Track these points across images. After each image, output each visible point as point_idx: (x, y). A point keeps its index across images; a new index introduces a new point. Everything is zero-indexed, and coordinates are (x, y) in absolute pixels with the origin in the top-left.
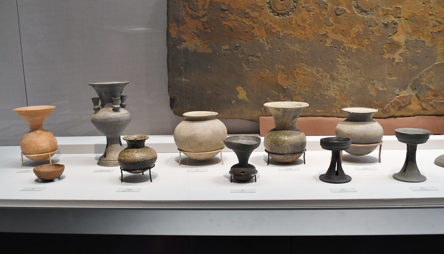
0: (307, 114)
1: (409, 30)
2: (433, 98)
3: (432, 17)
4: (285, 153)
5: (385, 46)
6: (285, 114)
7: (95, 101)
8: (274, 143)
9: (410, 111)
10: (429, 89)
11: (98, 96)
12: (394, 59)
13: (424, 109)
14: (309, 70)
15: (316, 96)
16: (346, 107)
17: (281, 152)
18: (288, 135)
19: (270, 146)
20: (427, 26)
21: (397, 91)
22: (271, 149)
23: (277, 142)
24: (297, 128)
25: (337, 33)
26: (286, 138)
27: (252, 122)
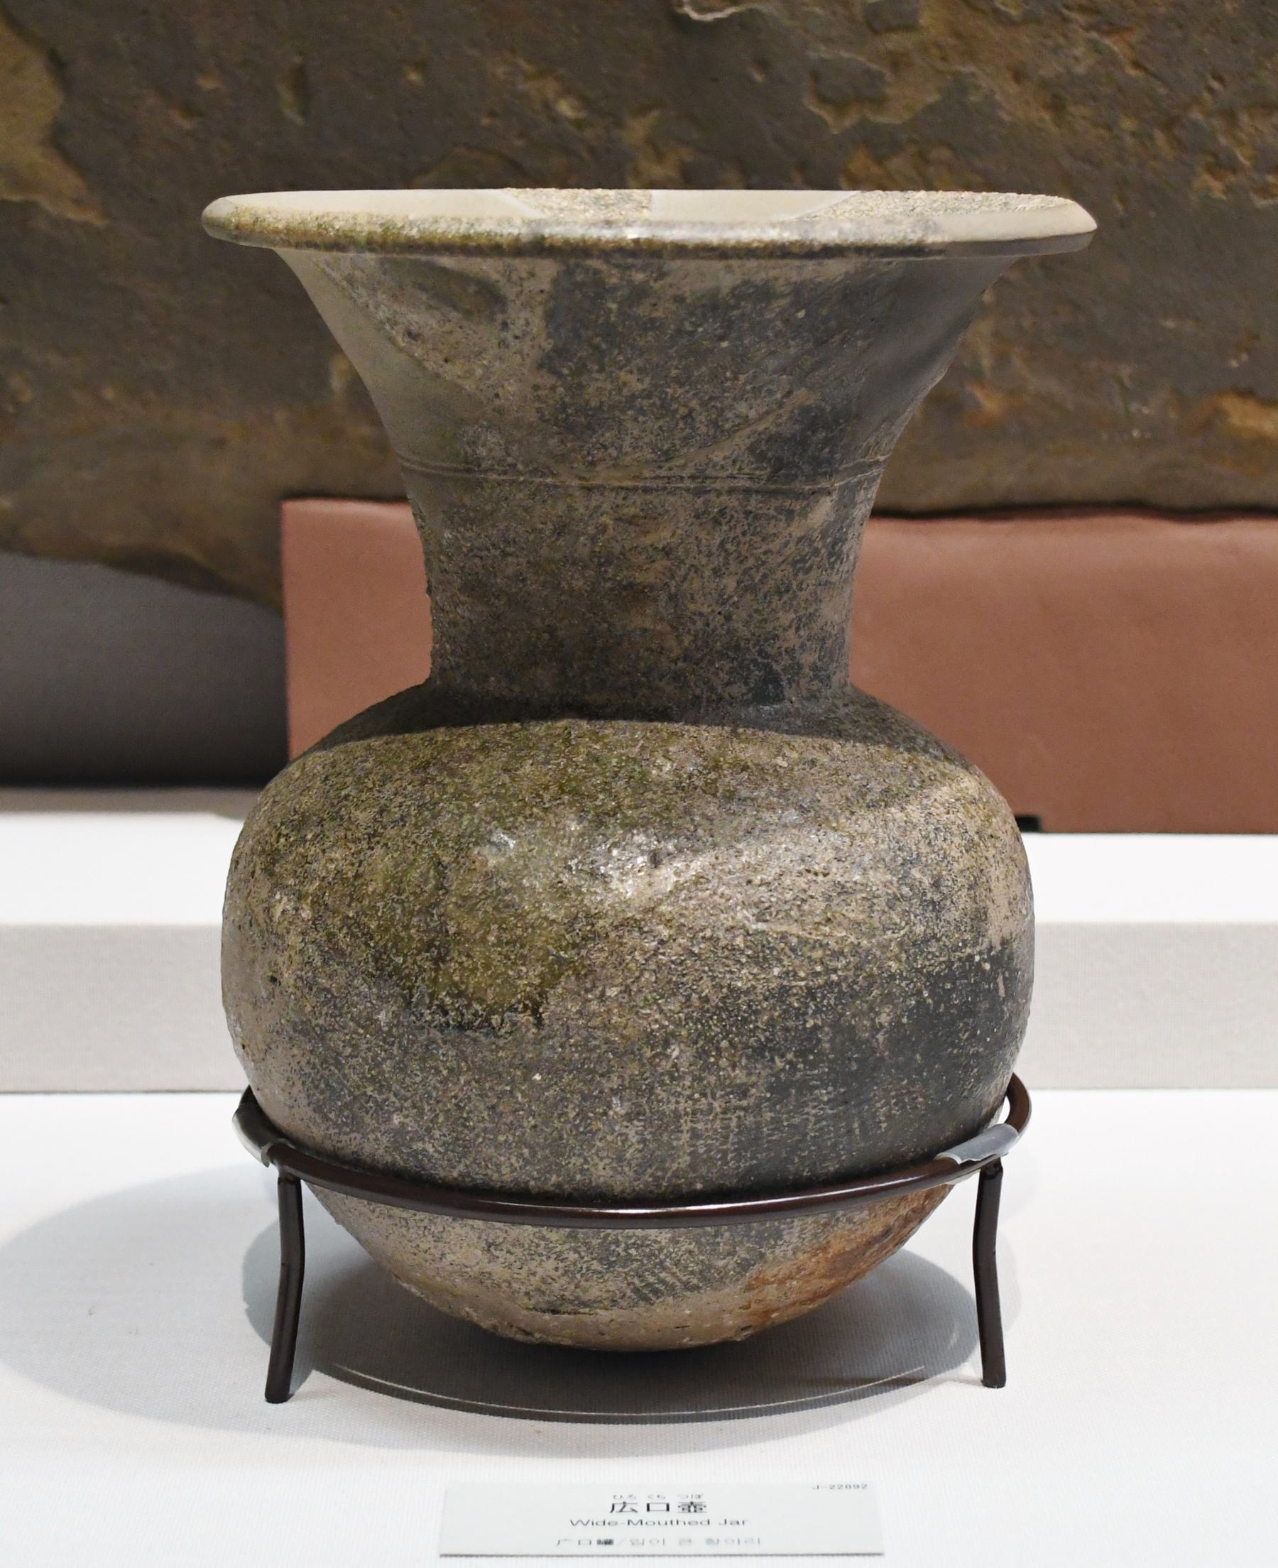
0: (1061, 473)
4: (602, 1173)
6: (597, 388)
8: (383, 971)
15: (1222, 165)
17: (507, 1168)
18: (673, 816)
19: (303, 1029)
22: (322, 1081)
23: (439, 948)
24: (864, 669)
26: (633, 877)
27: (157, 591)
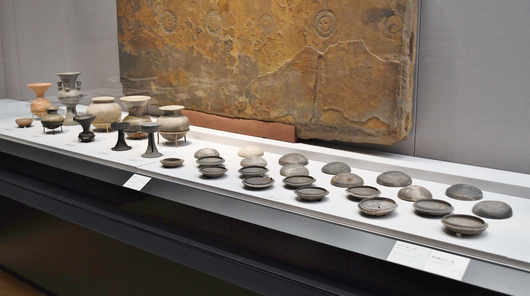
1: (240, 47)
2: (259, 105)
3: (254, 37)
5: (226, 59)
7: (60, 84)
9: (246, 115)
10: (256, 98)
11: (61, 81)
12: (233, 70)
13: (255, 114)
14: (186, 74)
16: (161, 106)
20: (251, 44)
21: (237, 97)
25: (199, 47)
